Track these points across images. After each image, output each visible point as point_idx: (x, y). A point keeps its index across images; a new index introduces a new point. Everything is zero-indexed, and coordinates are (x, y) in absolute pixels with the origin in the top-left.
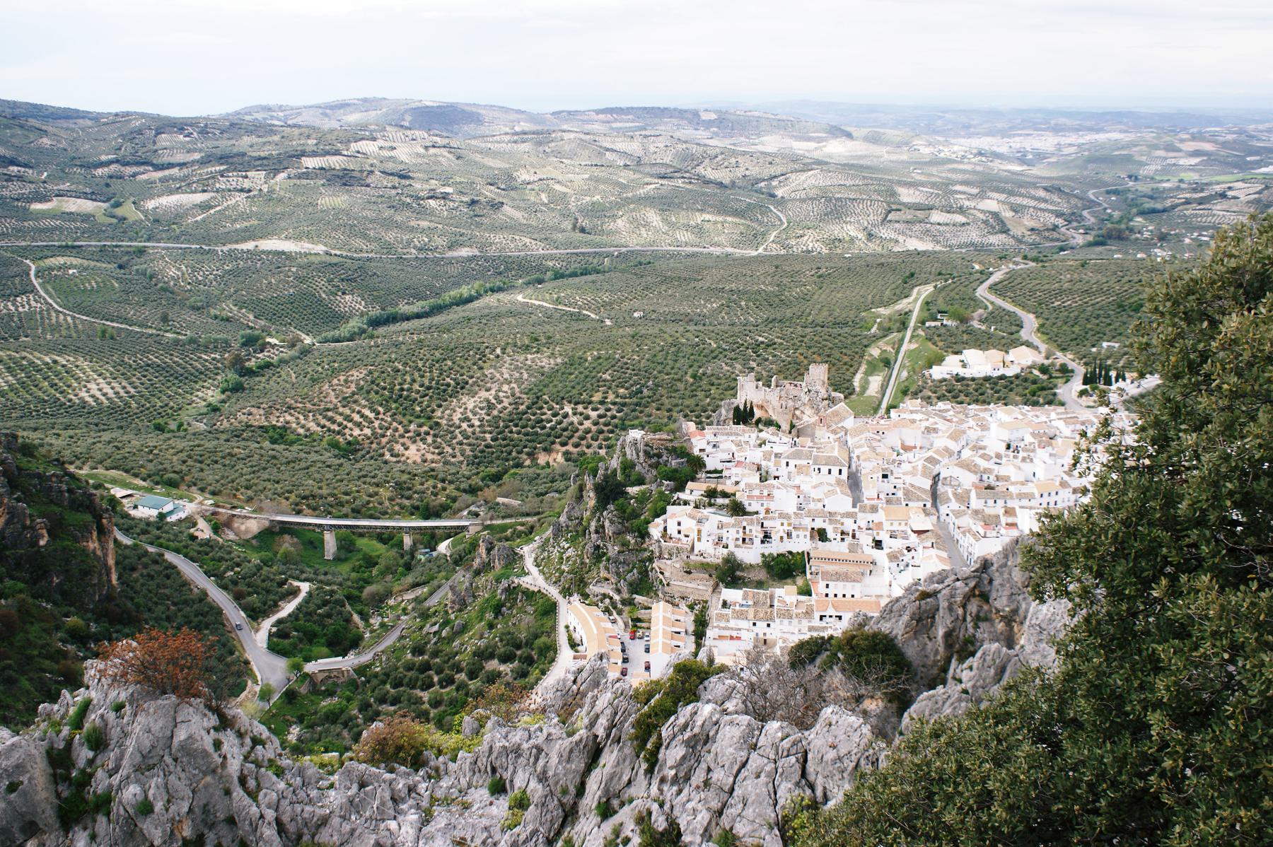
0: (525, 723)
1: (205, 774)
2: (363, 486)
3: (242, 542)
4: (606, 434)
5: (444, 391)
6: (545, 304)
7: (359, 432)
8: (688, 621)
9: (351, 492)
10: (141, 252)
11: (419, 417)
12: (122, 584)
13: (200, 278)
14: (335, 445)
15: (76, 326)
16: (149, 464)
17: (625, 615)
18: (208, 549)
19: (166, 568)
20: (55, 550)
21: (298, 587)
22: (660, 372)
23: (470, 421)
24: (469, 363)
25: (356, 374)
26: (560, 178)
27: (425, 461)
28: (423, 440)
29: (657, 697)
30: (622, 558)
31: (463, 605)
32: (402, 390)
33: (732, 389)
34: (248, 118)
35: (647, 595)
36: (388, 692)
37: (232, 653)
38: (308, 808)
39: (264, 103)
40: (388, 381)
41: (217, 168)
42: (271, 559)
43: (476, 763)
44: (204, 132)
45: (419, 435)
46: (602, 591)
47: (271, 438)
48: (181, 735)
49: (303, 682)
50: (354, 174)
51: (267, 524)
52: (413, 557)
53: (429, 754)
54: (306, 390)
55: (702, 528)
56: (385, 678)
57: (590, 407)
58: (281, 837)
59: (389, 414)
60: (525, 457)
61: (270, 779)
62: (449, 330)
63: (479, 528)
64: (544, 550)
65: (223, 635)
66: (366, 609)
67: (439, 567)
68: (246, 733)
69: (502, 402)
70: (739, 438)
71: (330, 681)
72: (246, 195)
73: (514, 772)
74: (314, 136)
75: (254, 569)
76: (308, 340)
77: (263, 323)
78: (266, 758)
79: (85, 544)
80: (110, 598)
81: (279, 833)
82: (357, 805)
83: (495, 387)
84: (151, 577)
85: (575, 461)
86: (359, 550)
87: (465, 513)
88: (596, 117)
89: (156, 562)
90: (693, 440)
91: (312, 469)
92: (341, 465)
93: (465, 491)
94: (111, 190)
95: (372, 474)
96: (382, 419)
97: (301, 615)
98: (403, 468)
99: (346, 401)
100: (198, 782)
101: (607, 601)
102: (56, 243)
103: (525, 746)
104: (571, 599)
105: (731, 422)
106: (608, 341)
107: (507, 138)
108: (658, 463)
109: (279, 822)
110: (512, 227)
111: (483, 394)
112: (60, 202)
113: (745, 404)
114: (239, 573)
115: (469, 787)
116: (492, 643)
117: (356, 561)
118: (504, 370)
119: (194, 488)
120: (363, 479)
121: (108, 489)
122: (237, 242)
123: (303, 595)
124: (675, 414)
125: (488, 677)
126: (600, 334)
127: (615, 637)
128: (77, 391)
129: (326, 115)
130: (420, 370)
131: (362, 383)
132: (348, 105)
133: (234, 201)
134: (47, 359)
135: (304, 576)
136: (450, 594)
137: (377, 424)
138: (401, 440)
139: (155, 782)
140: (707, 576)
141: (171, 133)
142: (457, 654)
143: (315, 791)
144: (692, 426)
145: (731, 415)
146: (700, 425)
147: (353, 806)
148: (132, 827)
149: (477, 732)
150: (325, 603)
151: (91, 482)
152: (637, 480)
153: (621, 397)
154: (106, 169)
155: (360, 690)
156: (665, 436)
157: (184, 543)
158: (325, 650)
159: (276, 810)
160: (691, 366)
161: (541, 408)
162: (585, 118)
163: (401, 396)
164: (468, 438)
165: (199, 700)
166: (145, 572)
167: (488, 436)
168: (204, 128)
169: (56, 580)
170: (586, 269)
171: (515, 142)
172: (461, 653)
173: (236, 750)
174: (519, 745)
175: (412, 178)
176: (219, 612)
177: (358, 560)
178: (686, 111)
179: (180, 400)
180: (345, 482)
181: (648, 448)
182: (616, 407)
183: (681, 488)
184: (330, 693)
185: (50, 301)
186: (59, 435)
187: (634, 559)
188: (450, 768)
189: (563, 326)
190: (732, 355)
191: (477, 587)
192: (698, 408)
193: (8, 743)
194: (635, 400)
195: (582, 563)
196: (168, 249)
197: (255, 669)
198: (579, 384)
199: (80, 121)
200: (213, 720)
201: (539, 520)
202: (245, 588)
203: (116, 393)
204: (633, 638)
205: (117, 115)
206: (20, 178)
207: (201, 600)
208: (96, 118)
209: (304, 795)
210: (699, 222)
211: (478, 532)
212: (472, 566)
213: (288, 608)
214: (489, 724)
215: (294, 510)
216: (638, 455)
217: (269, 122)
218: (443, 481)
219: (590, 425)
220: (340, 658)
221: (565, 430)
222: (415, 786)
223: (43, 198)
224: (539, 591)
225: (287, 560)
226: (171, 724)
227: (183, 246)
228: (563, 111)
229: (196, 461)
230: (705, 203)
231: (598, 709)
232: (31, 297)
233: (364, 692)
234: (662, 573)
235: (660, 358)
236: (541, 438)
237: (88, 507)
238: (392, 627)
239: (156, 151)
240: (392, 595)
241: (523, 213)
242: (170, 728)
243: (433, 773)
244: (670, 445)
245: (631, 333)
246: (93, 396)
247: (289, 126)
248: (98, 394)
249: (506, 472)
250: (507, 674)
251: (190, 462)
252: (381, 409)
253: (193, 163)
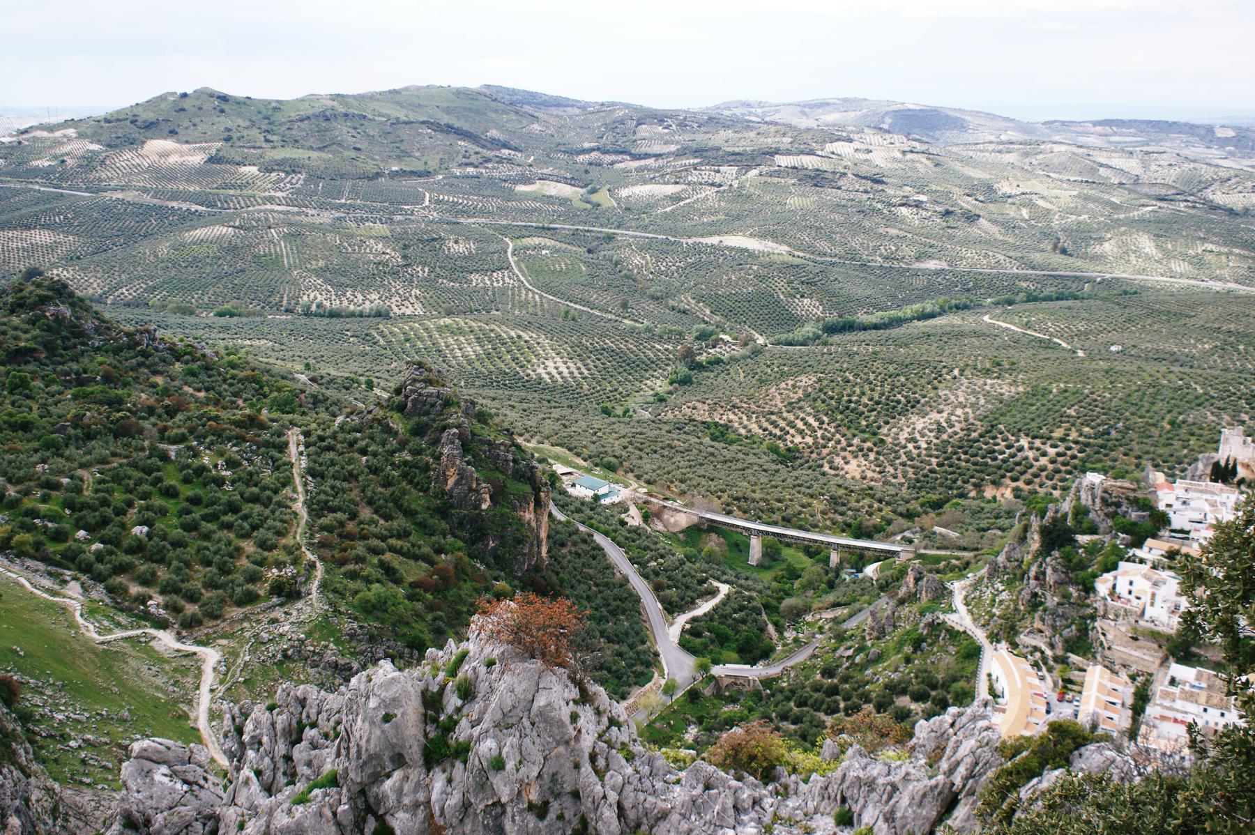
0: (889, 757)
1: (558, 744)
2: (797, 495)
3: (668, 534)
4: (1063, 475)
5: (894, 408)
6: (1012, 327)
7: (801, 440)
8: (1127, 692)
9: (784, 500)
10: (610, 238)
11: (863, 431)
12: (551, 557)
13: (663, 269)
14: (774, 450)
15: (542, 305)
16: (592, 445)
17: (1056, 673)
18: (636, 537)
19: (594, 549)
20: (495, 515)
21: (718, 588)
22: (1133, 414)
23: (916, 442)
24: (923, 381)
25: (805, 380)
26: (1045, 193)
27: (864, 478)
29: (1025, 754)
30: (1060, 611)
31: (882, 633)
32: (850, 401)
33: (1214, 442)
34: (727, 113)
35: (1084, 655)
36: (791, 710)
37: (643, 642)
38: (651, 799)
39: (744, 99)
40: (836, 391)
41: (692, 161)
42: (695, 556)
43: (826, 789)
44: (683, 125)
45: (861, 450)
46: (1034, 643)
47: (712, 434)
48: (541, 701)
49: (708, 684)
50: (826, 175)
51: (696, 520)
52: (838, 576)
53: (782, 770)
54: (752, 390)
55: (1156, 592)
56: (790, 694)
57: (1049, 443)
58: (620, 821)
59: (833, 425)
60: (971, 487)
61: (620, 762)
62: (906, 345)
63: (911, 556)
64: (976, 589)
65: (637, 623)
66: (782, 621)
67: (863, 589)
68: (605, 712)
69: (953, 426)
70: (1216, 498)
71: (735, 688)
72: (716, 189)
73: (864, 806)
74: (790, 134)
75: (677, 563)
76: (761, 340)
77: (718, 318)
78: (619, 741)
79: (522, 513)
80: (537, 569)
81: (619, 817)
82: (699, 806)
83: (948, 409)
84: (578, 555)
85: (1024, 499)
86: (784, 561)
87: (899, 538)
88: (1092, 129)
89: (584, 541)
90: (1160, 493)
91: (750, 471)
92: (777, 471)
93: (901, 515)
94: (589, 176)
95: (808, 484)
96: (826, 429)
97: (716, 616)
98: (841, 482)
99: (791, 407)
100: (551, 750)
101: (1038, 655)
102: (534, 224)
103: (881, 781)
104: (999, 646)
105: (1208, 479)
106: (1078, 374)
107: (991, 147)
108: (1116, 513)
109: (620, 805)
110: (986, 243)
111: (934, 416)
112: (542, 185)
113: (1228, 460)
114: (662, 564)
115: (816, 811)
116: (906, 678)
117: (779, 570)
118: (959, 393)
119: (630, 474)
120: (798, 488)
121: (551, 465)
122: (702, 236)
123: (721, 597)
124: (1144, 462)
125: (897, 712)
126: (1069, 365)
127: (1041, 695)
128: (535, 367)
129: (804, 113)
130: (871, 383)
131: (810, 390)
132: (828, 104)
133: (704, 195)
134: (513, 334)
135: (725, 577)
136: (870, 620)
137: (819, 433)
138: (843, 454)
139: (511, 741)
140: (1155, 646)
141: (651, 124)
142: (867, 683)
143: (661, 783)
144: (1160, 477)
145: (1209, 471)
146: (1171, 478)
147: (695, 805)
148: (484, 779)
149: (837, 758)
150: (742, 608)
151: (536, 455)
152: (1088, 528)
153: (1086, 437)
154: (587, 156)
155: (764, 702)
156: (1127, 485)
157: (614, 527)
158: (735, 655)
159: (620, 794)
160: (1169, 412)
161: (995, 438)
162: (1080, 129)
163: (847, 408)
165: (563, 670)
166: (573, 549)
167: (934, 460)
168: (683, 121)
169: (492, 544)
170: (1062, 293)
171: (1000, 152)
172: (872, 683)
173: (592, 727)
174: (875, 779)
175: (886, 184)
176: (637, 600)
177: (782, 570)
178: (1198, 127)
179: (629, 387)
180: (780, 489)
181: (1106, 496)
182: (1078, 447)
183: (1139, 544)
184: (733, 700)
185: (522, 279)
186: (513, 407)
187: (1074, 614)
188: (800, 789)
189: (1031, 352)
190: (1221, 404)
191: (899, 617)
192: (1173, 459)
193: (389, 676)
194: (1100, 441)
195: (1016, 609)
196: (636, 237)
197: (663, 662)
198: (1039, 416)
199: (569, 109)
200: (574, 693)
201: (976, 556)
202: (665, 580)
203: (571, 373)
204: (1060, 700)
205: (603, 104)
206: (510, 161)
207: (621, 586)
208: (584, 107)
209: (650, 785)
210: (1200, 251)
211: (909, 560)
212: (897, 594)
213: (704, 607)
214: (850, 752)
215: (724, 509)
216: (1094, 501)
217: (747, 118)
218: (880, 501)
219: (1046, 463)
220: (748, 667)
221: (1018, 464)
222: (761, 799)
223: (527, 181)
224: (965, 632)
225: (710, 559)
226: (534, 689)
227: (650, 235)
228: (1056, 121)
229: (636, 448)
230: (1208, 231)
231: (959, 755)
232: (506, 274)
233: (767, 705)
234: (1104, 634)
235: (1134, 398)
236: (990, 470)
237: (529, 479)
238: (806, 643)
239: (635, 141)
240: (810, 611)
241: (999, 228)
242: (532, 693)
243: (781, 790)
244: (1132, 495)
245: (1105, 368)
246: (549, 373)
247: (766, 123)
248: (554, 372)
249: (947, 501)
250: (917, 714)
251: (630, 449)
252: (826, 419)
253: (669, 154)
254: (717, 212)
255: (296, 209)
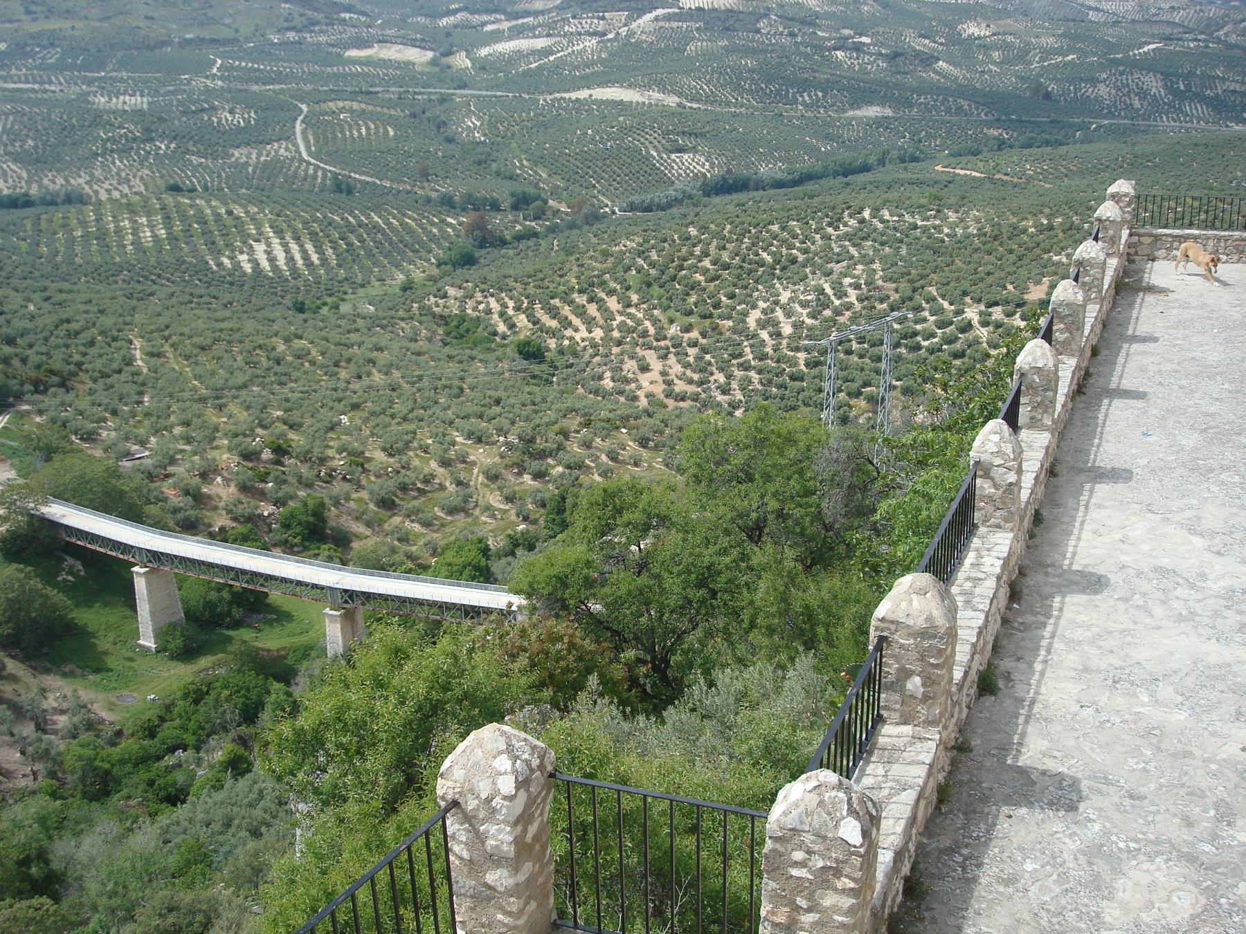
28: (681, 355)
50: (741, 16)
112: (381, 48)
122: (568, 91)
154: (452, 18)
161: (918, 309)
164: (763, 357)
223: (361, 43)
254: (594, 63)
255: (36, 87)
